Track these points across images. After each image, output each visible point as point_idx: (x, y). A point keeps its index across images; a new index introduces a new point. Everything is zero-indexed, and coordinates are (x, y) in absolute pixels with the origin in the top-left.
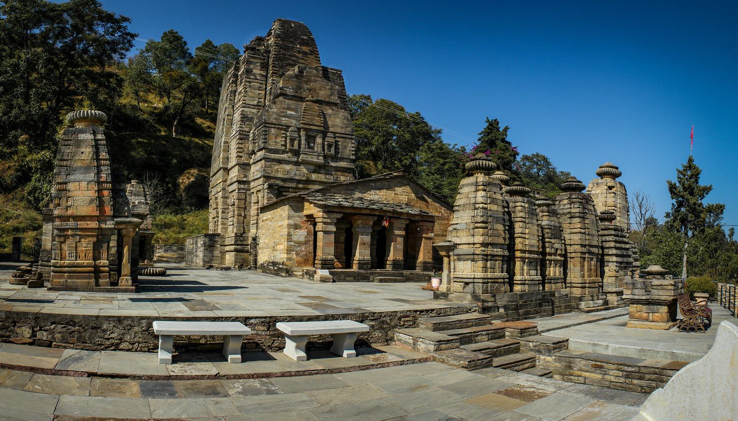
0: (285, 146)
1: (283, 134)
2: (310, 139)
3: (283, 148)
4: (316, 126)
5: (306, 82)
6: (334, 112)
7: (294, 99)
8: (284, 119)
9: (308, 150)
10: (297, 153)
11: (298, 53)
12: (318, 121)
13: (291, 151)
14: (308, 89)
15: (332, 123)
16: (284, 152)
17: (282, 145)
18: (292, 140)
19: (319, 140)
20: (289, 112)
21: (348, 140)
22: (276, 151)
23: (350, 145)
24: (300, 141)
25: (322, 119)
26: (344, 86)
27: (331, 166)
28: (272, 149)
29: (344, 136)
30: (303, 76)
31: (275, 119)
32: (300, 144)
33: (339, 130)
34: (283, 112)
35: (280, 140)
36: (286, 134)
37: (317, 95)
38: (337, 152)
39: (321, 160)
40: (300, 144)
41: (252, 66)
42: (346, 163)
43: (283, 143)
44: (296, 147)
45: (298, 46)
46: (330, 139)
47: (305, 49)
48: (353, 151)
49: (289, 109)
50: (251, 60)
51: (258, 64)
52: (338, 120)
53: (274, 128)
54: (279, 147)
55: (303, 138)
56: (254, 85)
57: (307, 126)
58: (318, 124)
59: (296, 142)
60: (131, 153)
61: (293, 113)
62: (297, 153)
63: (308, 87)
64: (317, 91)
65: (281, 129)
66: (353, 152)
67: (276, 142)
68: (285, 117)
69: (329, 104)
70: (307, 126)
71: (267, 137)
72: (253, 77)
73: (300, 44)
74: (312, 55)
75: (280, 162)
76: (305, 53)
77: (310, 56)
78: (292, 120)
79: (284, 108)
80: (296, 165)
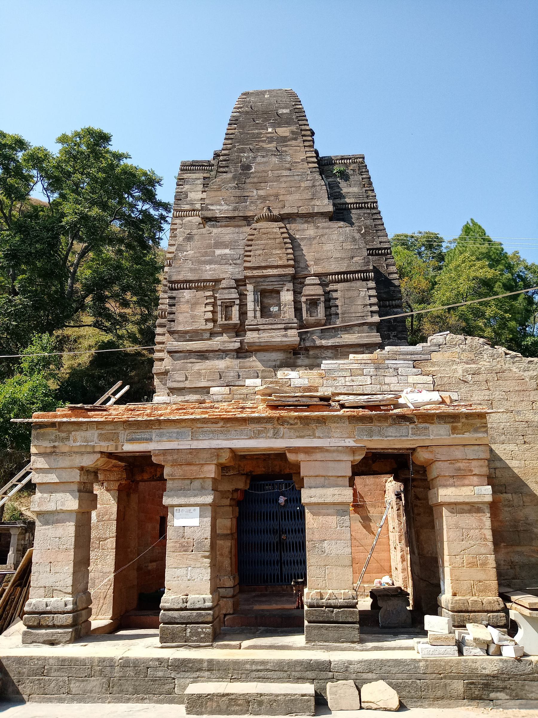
0: (214, 321)
1: (207, 297)
2: (267, 296)
3: (210, 325)
4: (277, 267)
5: (257, 186)
6: (320, 232)
7: (232, 223)
8: (208, 267)
9: (264, 321)
10: (239, 330)
11: (270, 142)
12: (280, 256)
13: (226, 329)
14: (260, 197)
15: (317, 256)
16: (212, 334)
17: (207, 320)
18: (227, 306)
19: (287, 297)
20: (218, 252)
21: (359, 283)
22: (194, 335)
23: (362, 294)
24: (243, 306)
25: (291, 251)
26: (371, 184)
27: (321, 347)
28: (186, 332)
29: (345, 277)
30: (248, 176)
31: (191, 270)
32: (243, 314)
33: (334, 267)
34: (206, 254)
35: (203, 312)
36: (215, 298)
37: (280, 205)
38: (329, 316)
39: (292, 337)
40: (243, 314)
41: (186, 187)
42: (357, 335)
43: (210, 315)
44: (235, 319)
45: (270, 130)
46: (313, 289)
47: (284, 131)
48: (371, 305)
49: (219, 245)
50: (185, 176)
51: (199, 182)
52: (328, 247)
53: (190, 288)
54: (201, 325)
55: (250, 298)
56: (189, 221)
57: (256, 273)
58: (280, 263)
59: (235, 311)
60: (271, 310)
61: (227, 251)
62: (239, 330)
63: (261, 193)
64: (281, 198)
65: (205, 288)
66: (375, 308)
67: (193, 317)
68: (210, 262)
69: (309, 217)
70: (256, 273)
71: (174, 309)
72: (187, 207)
73: (274, 126)
74: (295, 139)
75: (203, 355)
76: (283, 140)
77: (293, 143)
78: (226, 267)
79: (209, 246)
80: (238, 358)
